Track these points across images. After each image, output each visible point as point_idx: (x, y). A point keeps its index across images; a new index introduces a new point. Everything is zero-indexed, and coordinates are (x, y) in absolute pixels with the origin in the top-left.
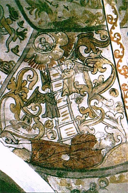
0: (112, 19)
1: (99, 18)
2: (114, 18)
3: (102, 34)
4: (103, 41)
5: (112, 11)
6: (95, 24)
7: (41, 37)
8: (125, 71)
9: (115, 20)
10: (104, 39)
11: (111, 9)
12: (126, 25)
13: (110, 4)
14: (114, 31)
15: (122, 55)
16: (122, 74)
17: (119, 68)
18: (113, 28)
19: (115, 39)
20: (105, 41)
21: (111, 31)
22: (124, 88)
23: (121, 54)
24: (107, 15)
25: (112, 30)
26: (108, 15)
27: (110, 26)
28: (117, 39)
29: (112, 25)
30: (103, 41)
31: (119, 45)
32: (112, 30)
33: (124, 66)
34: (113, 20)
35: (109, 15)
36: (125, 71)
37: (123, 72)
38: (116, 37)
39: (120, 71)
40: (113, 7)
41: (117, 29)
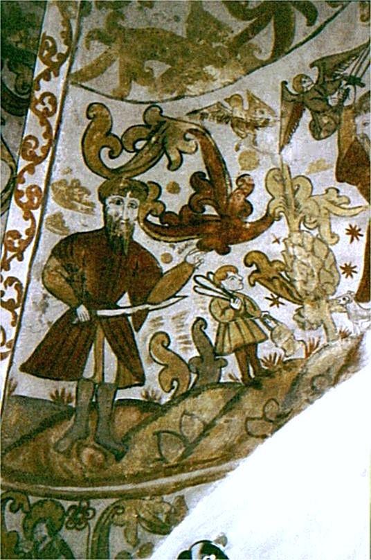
0: (53, 50)
1: (30, 30)
2: (59, 52)
3: (24, 77)
4: (19, 96)
5: (60, 31)
6: (16, 40)
7: (308, 101)
8: (31, 200)
9: (58, 58)
10: (20, 90)
11: (60, 24)
12: (91, 84)
13: (63, 10)
14: (45, 86)
15: (40, 157)
16: (20, 204)
17: (20, 187)
18: (46, 76)
19: (40, 107)
20: (23, 99)
21: (38, 80)
22: (10, 241)
23: (39, 153)
24: (44, 34)
25: (42, 81)
26: (47, 34)
27: (40, 68)
28: (47, 109)
29: (45, 67)
30: (19, 96)
31: (44, 129)
32: (42, 81)
33: (35, 186)
34: (55, 54)
35: (51, 39)
36: (31, 200)
37: (25, 199)
38: (44, 104)
39: (21, 194)
40: (67, 23)
41: (55, 85)
